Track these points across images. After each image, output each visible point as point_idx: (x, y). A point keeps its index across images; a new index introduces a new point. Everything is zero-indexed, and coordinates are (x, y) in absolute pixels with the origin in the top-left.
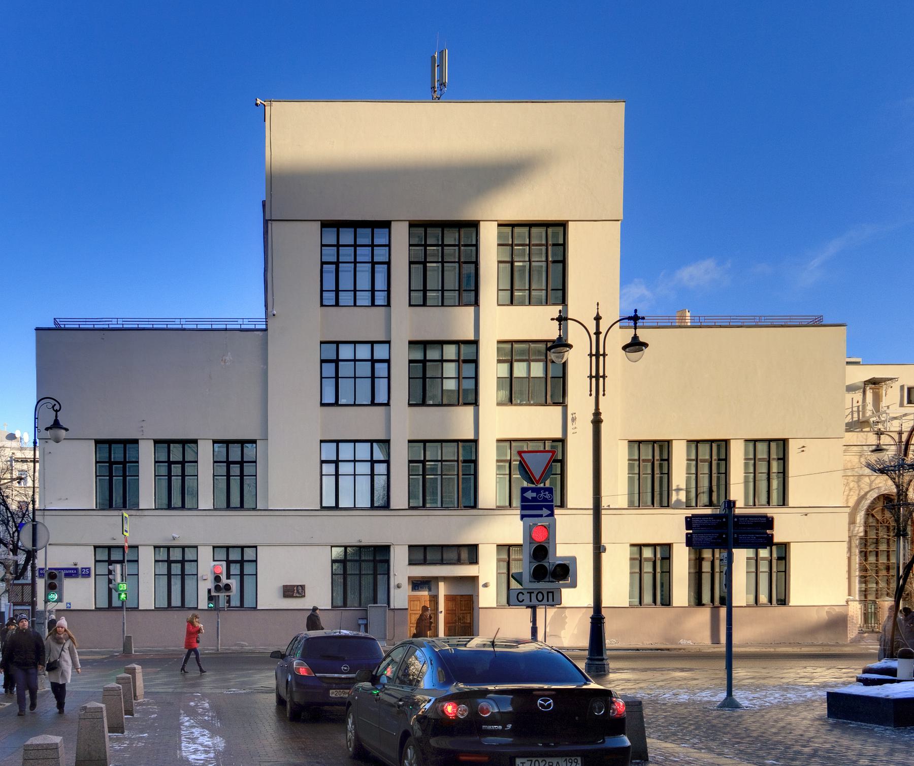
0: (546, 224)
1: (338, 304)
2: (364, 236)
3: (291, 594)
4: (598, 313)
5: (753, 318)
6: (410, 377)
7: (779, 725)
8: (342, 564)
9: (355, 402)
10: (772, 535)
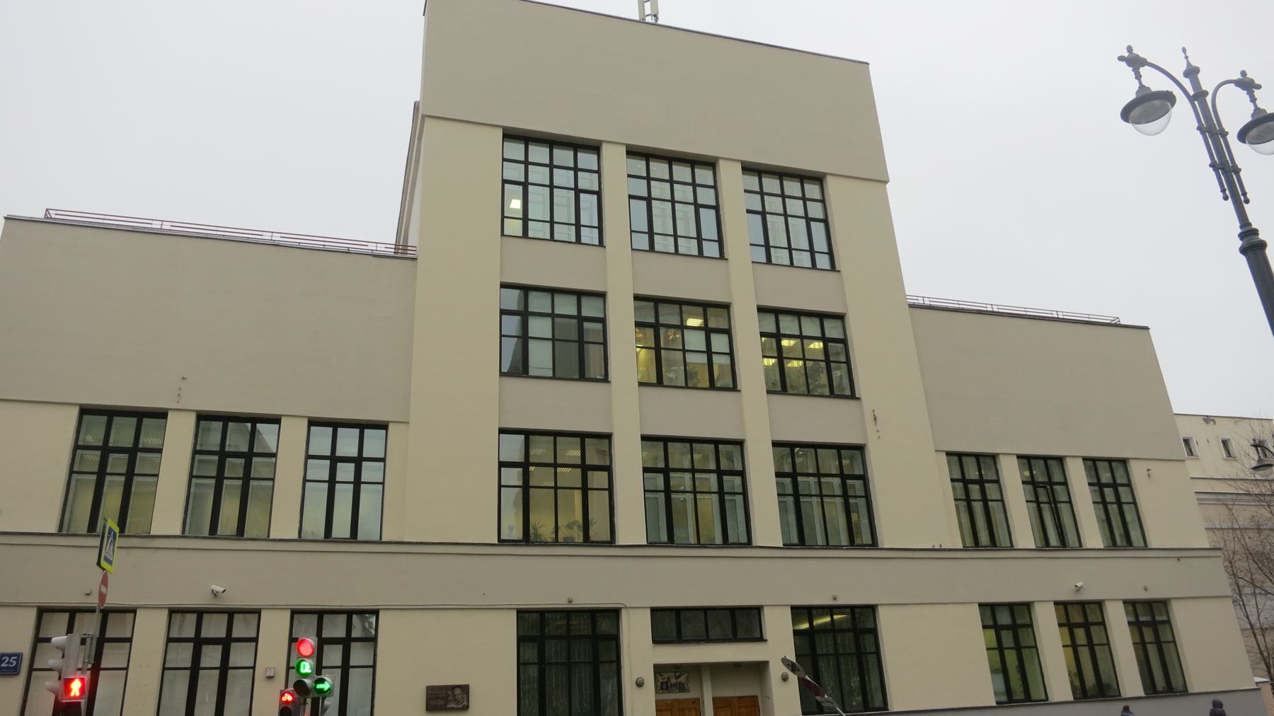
0: (836, 446)
1: (584, 375)
2: (564, 156)
3: (442, 702)
4: (1189, 64)
5: (916, 298)
6: (632, 229)
7: (1243, 457)
8: (45, 614)
9: (601, 344)
10: (1224, 711)
